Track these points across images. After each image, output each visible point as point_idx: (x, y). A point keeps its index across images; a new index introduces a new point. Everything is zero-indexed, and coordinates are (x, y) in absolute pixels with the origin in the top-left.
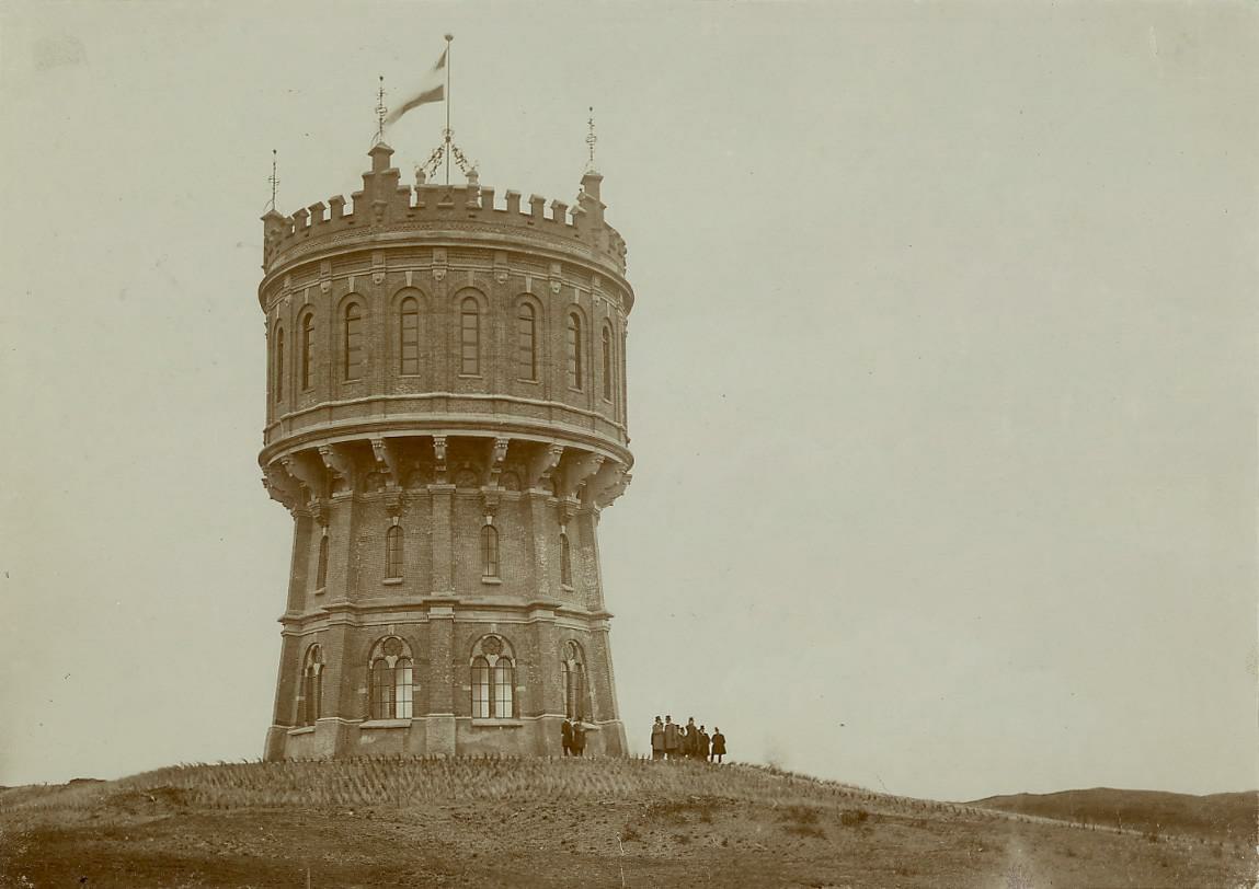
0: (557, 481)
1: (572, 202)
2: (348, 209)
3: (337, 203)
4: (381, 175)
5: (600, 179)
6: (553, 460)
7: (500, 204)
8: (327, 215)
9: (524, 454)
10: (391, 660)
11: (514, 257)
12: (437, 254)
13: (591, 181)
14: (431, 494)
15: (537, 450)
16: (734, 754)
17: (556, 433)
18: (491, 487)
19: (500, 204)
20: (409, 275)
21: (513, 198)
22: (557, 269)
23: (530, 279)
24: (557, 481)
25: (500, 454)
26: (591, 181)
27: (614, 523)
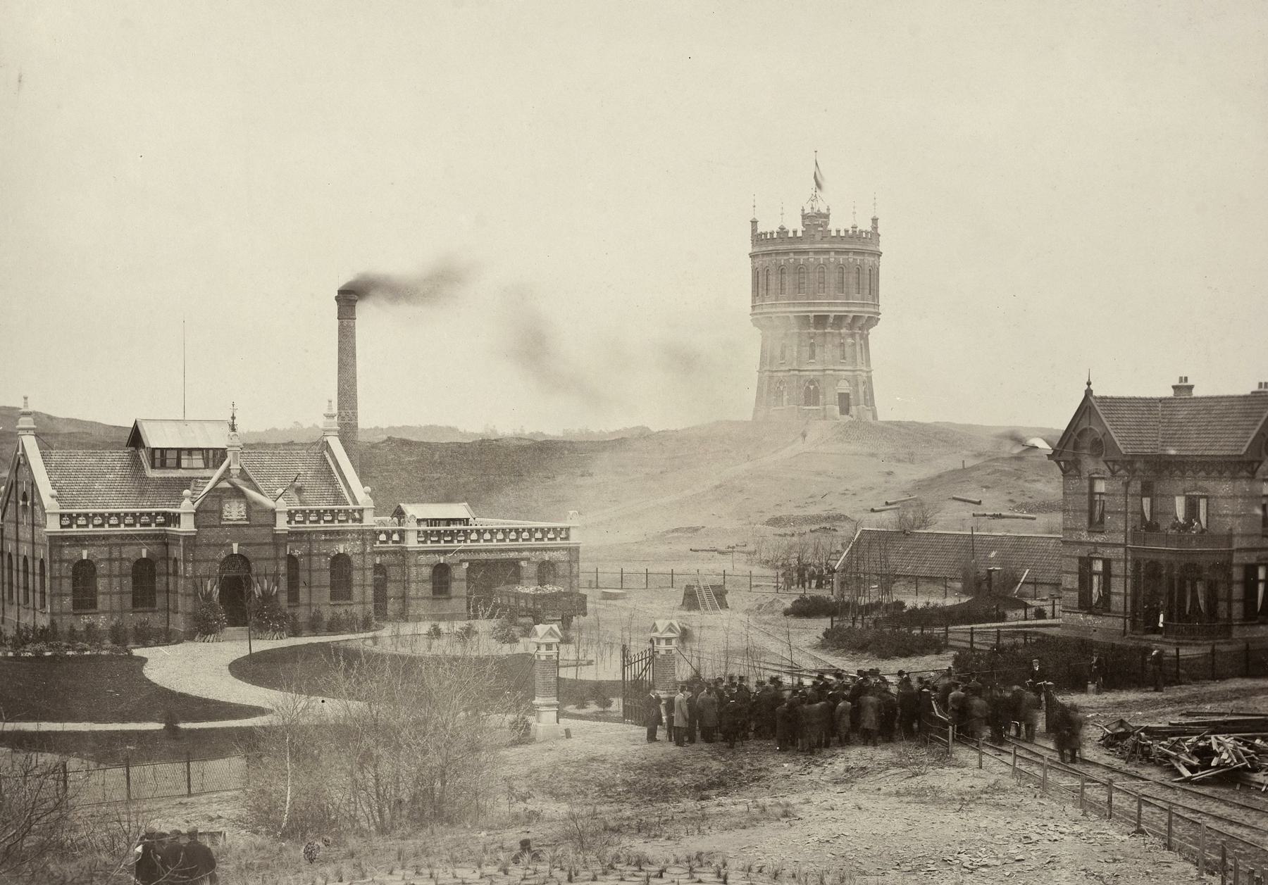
0: (851, 326)
1: (870, 229)
2: (775, 236)
3: (772, 233)
4: (816, 221)
5: (877, 219)
6: (849, 321)
7: (791, 235)
8: (768, 237)
9: (839, 319)
10: (781, 388)
11: (777, 254)
12: (811, 253)
13: (875, 220)
14: (825, 333)
15: (827, 317)
16: (1196, 393)
17: (811, 312)
18: (829, 330)
19: (791, 235)
20: (782, 261)
21: (838, 231)
22: (832, 254)
23: (802, 258)
24: (851, 326)
25: (831, 320)
26: (875, 220)
27: (874, 334)
